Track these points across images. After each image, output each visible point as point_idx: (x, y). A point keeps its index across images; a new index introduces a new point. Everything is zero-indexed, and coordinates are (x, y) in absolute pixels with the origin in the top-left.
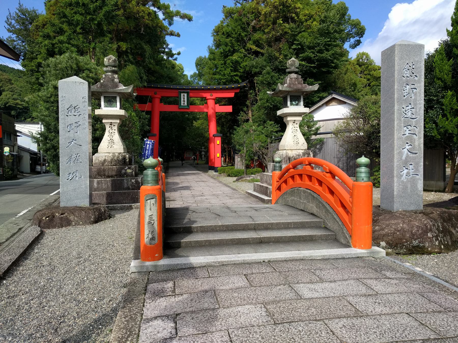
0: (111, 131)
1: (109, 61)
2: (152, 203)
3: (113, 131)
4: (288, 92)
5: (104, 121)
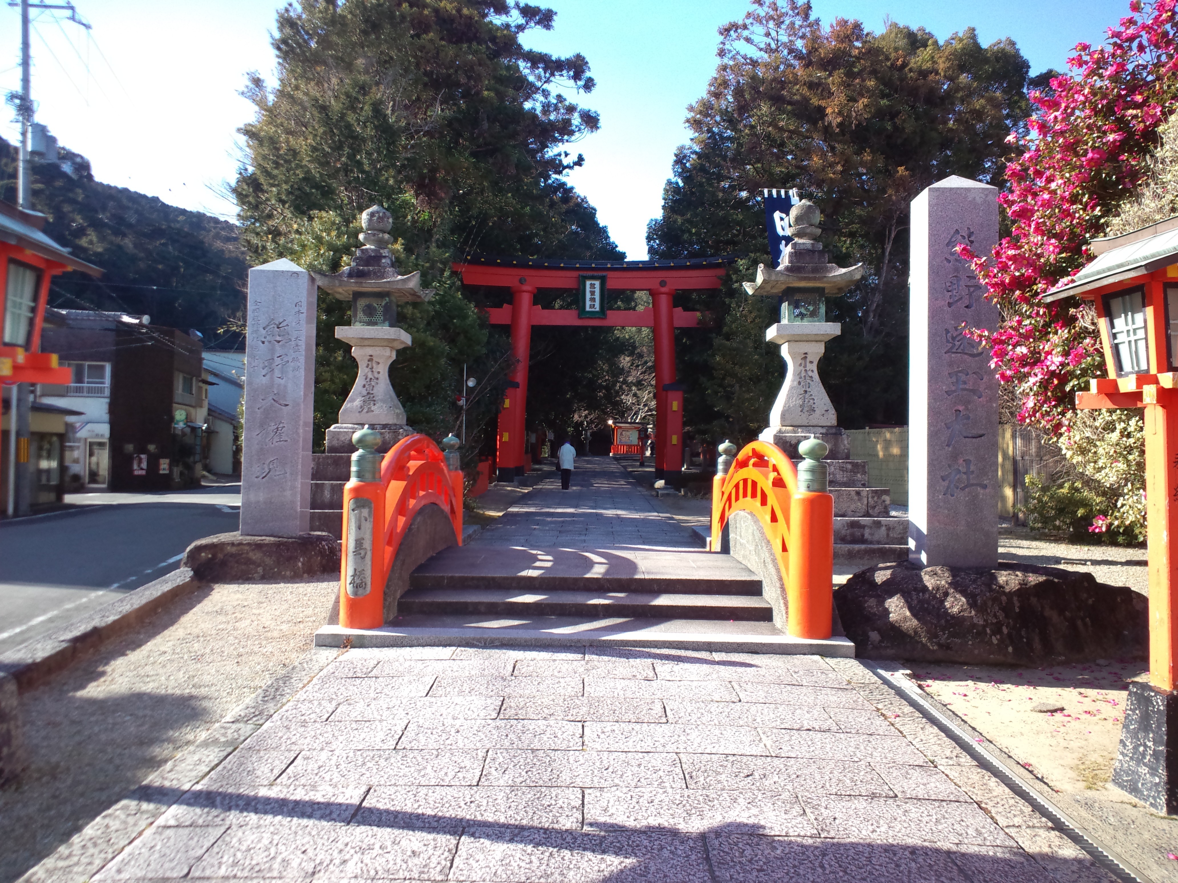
0: (370, 375)
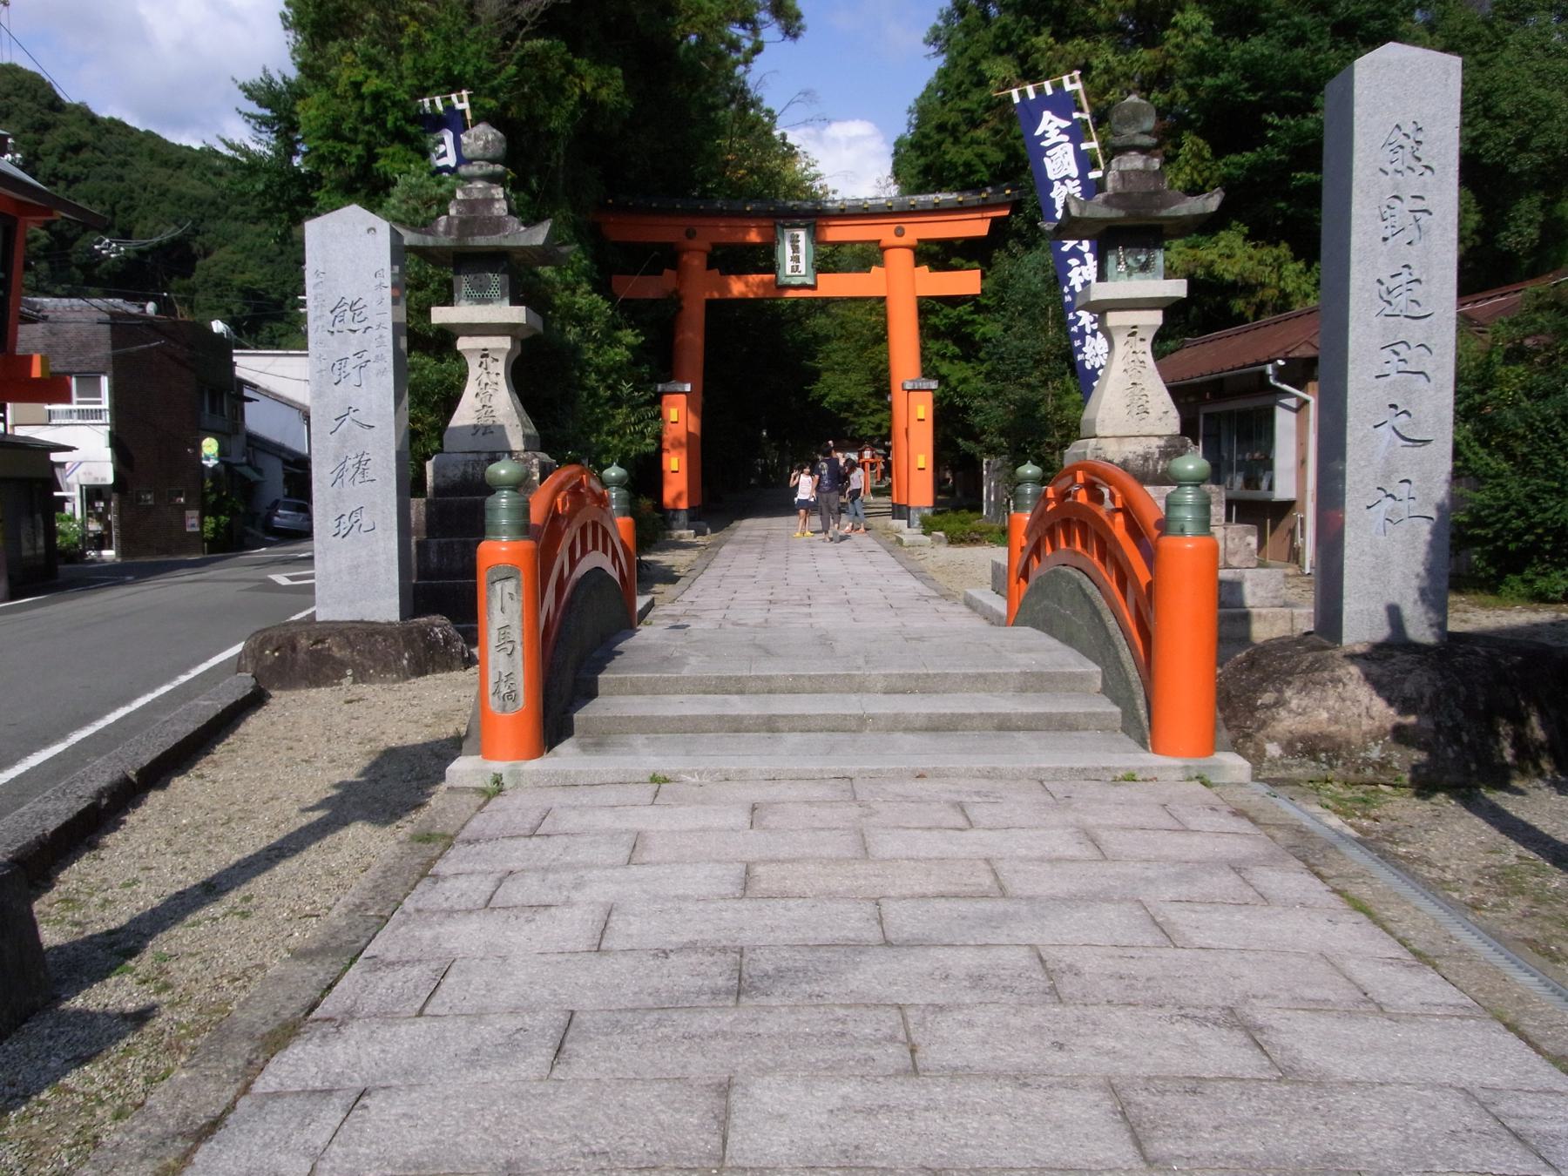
0: (485, 379)
2: (507, 590)
3: (493, 377)
5: (463, 344)
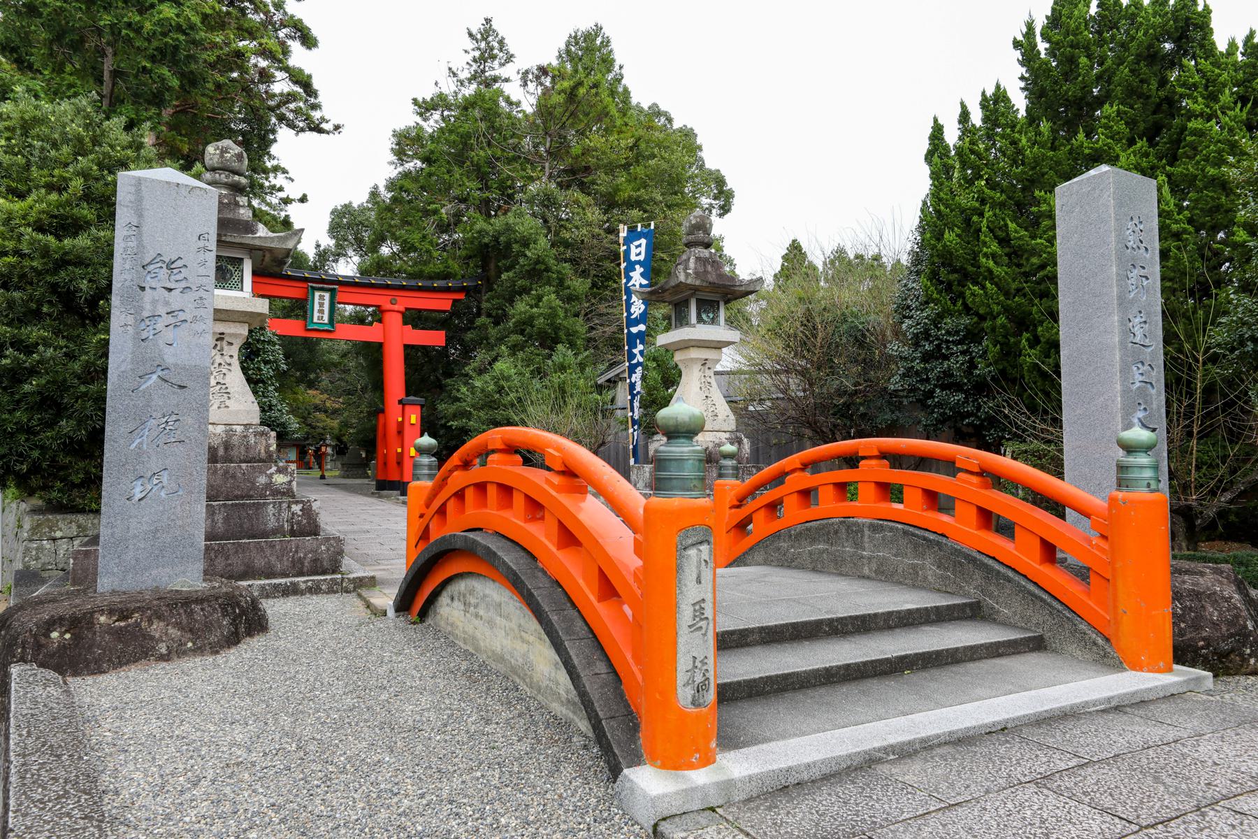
1: (222, 156)
4: (695, 290)
